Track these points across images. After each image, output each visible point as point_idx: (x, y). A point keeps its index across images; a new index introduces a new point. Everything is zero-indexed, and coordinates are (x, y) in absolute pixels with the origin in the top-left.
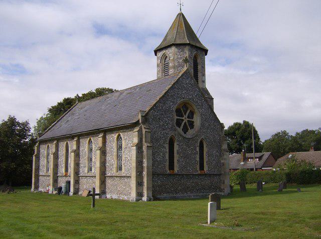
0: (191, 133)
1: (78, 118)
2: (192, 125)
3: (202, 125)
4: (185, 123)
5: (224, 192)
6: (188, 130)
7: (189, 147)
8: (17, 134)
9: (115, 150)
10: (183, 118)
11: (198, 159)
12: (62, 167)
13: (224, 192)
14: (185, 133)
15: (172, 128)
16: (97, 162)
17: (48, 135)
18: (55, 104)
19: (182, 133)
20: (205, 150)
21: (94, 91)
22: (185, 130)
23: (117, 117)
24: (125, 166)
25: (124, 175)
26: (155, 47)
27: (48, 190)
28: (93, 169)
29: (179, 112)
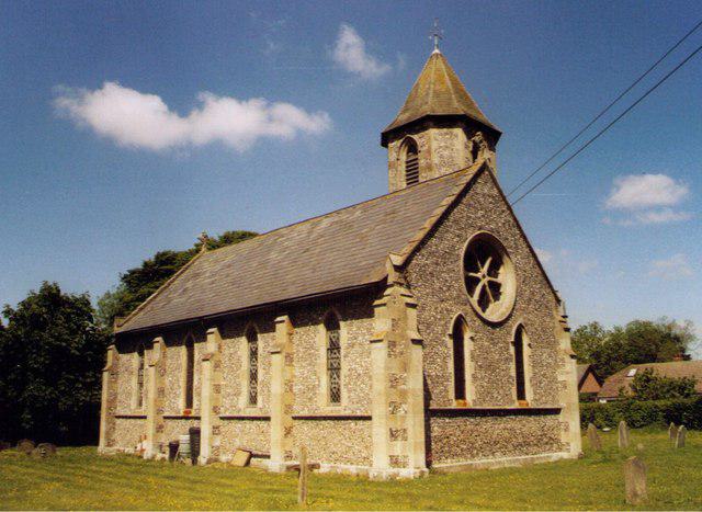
0: (495, 312)
1: (213, 283)
2: (496, 288)
3: (519, 293)
4: (484, 286)
5: (568, 450)
6: (488, 302)
7: (495, 344)
8: (27, 334)
9: (323, 352)
10: (479, 275)
11: (513, 373)
12: (176, 396)
13: (568, 450)
14: (484, 311)
15: (459, 297)
16: (273, 382)
17: (138, 320)
18: (140, 266)
19: (479, 310)
20: (526, 351)
21: (217, 239)
22: (484, 302)
23: (316, 274)
24: (349, 391)
25: (348, 413)
26: (385, 127)
27: (142, 450)
28: (260, 399)
29: (471, 263)
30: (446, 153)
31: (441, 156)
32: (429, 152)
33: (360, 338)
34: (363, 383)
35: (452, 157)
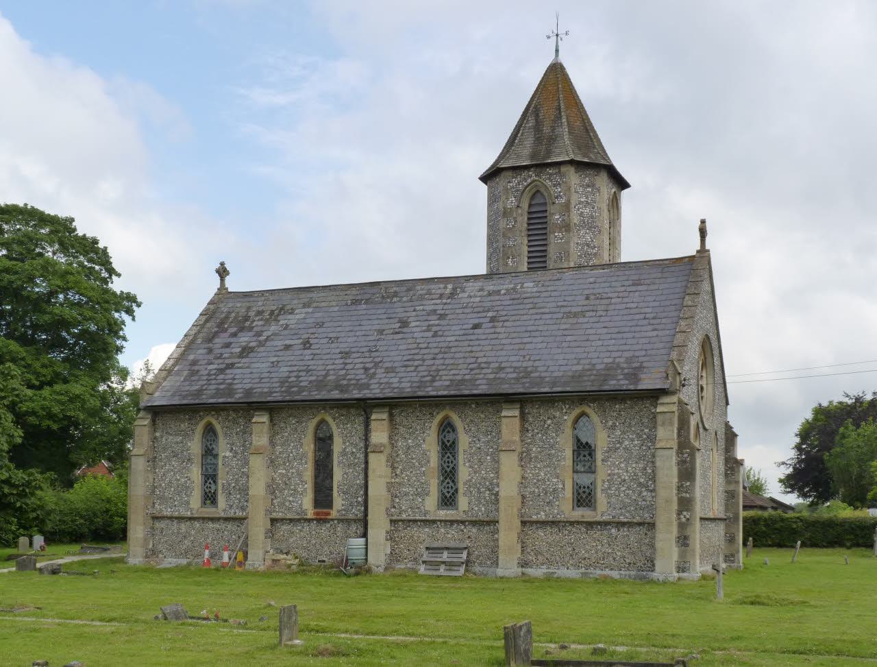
24: (609, 496)
30: (587, 211)
31: (581, 214)
32: (567, 206)
33: (626, 443)
34: (629, 488)
35: (592, 217)
